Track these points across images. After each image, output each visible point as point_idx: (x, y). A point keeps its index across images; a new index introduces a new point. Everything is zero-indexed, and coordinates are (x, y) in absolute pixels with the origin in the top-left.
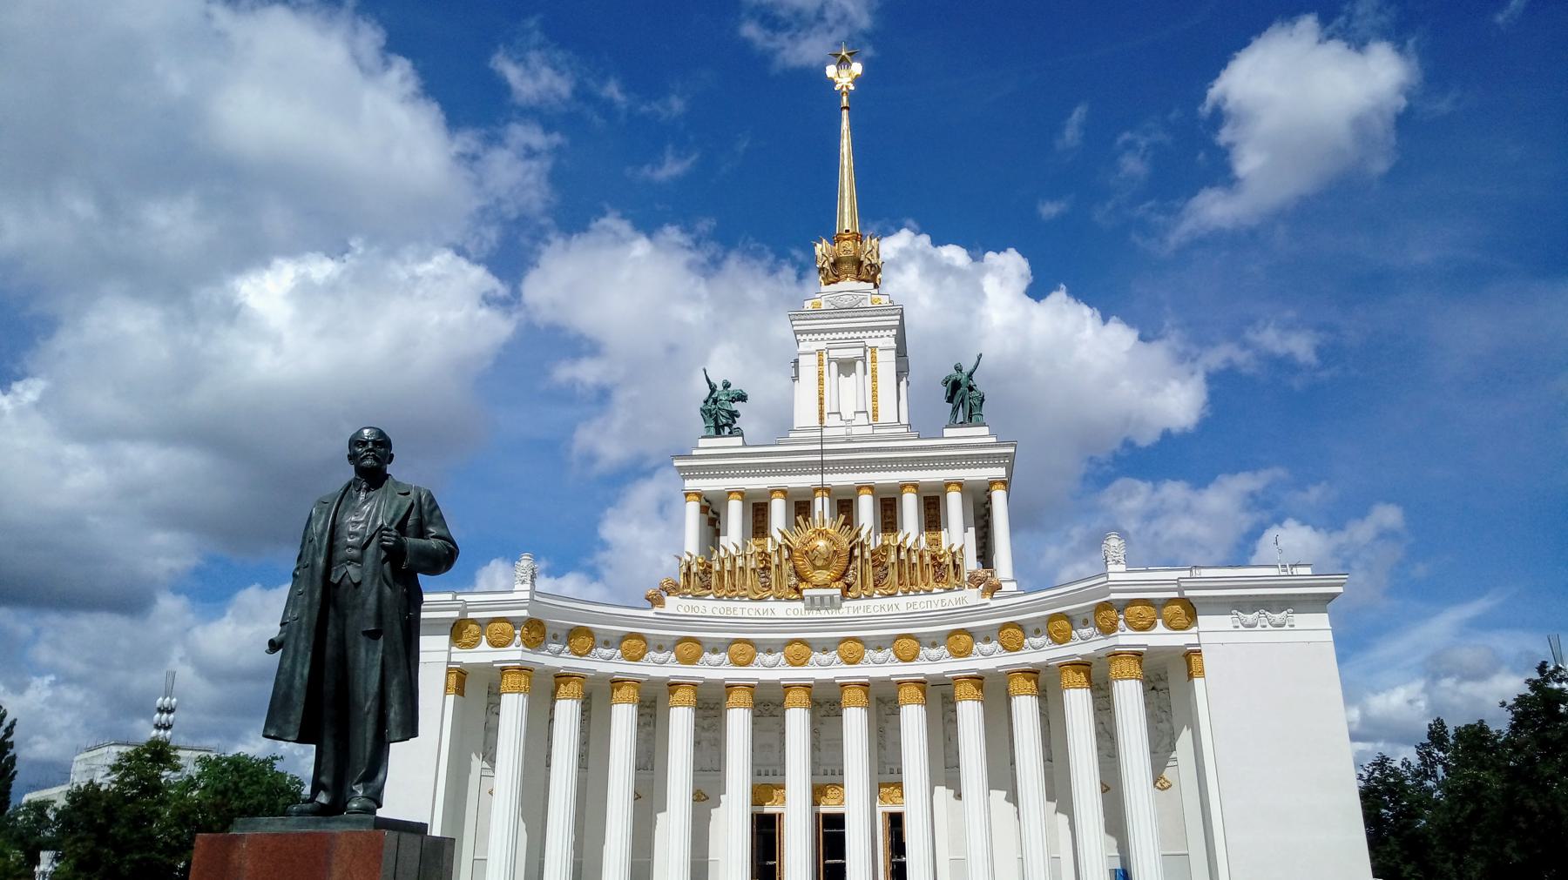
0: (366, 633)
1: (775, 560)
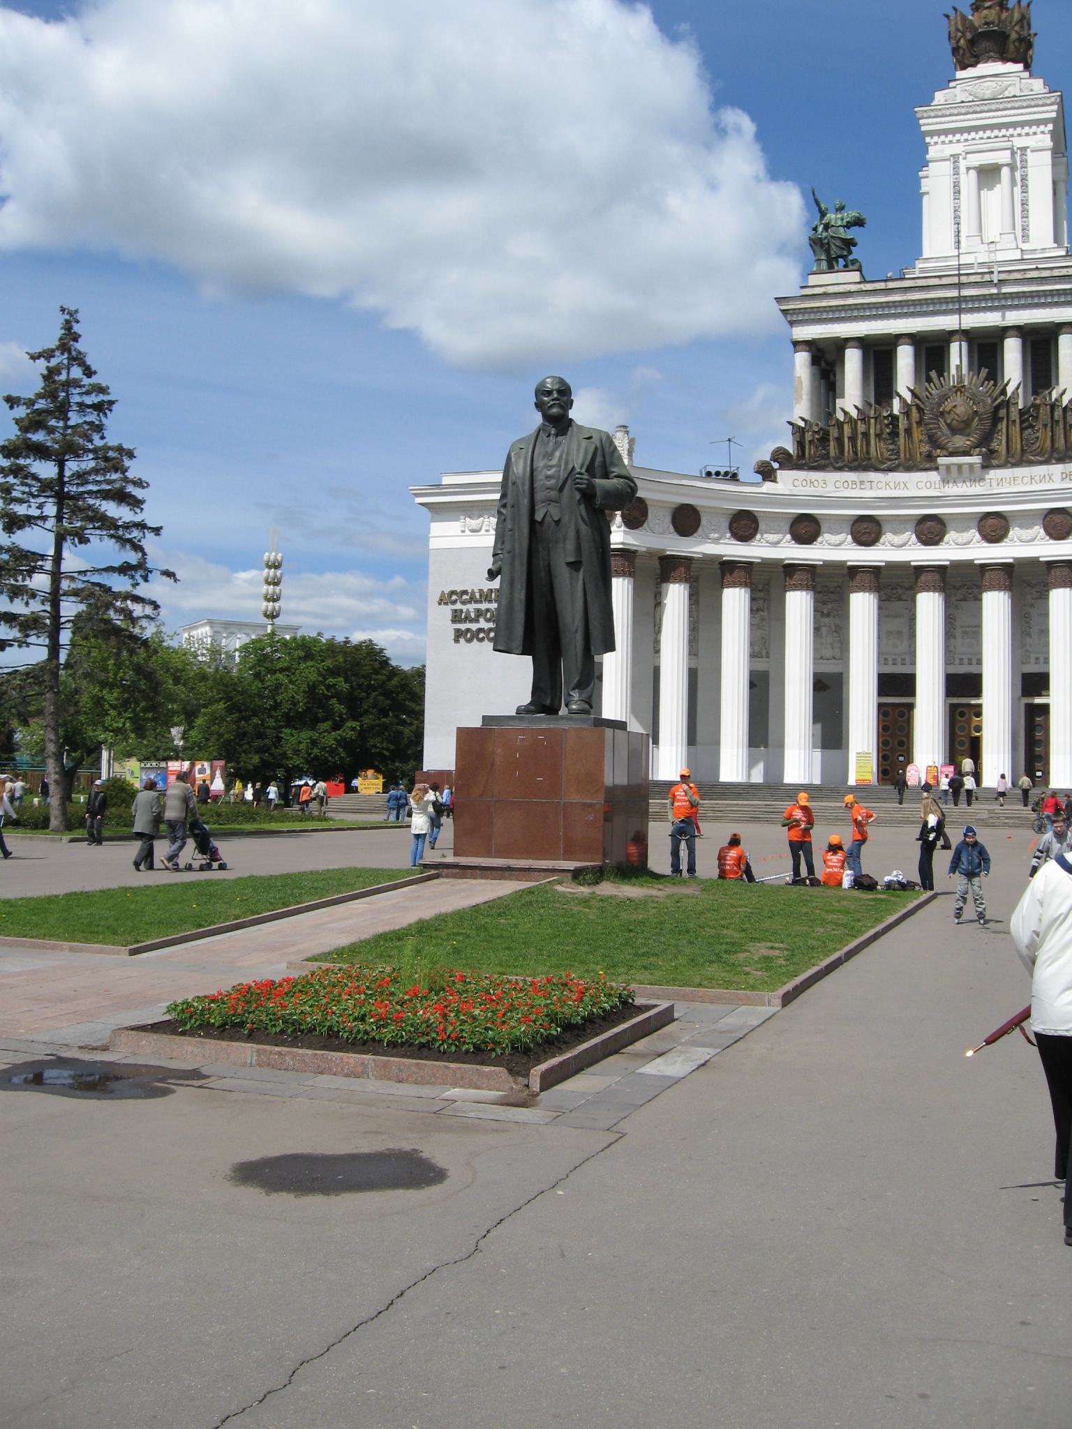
0: (569, 564)
1: (903, 424)
